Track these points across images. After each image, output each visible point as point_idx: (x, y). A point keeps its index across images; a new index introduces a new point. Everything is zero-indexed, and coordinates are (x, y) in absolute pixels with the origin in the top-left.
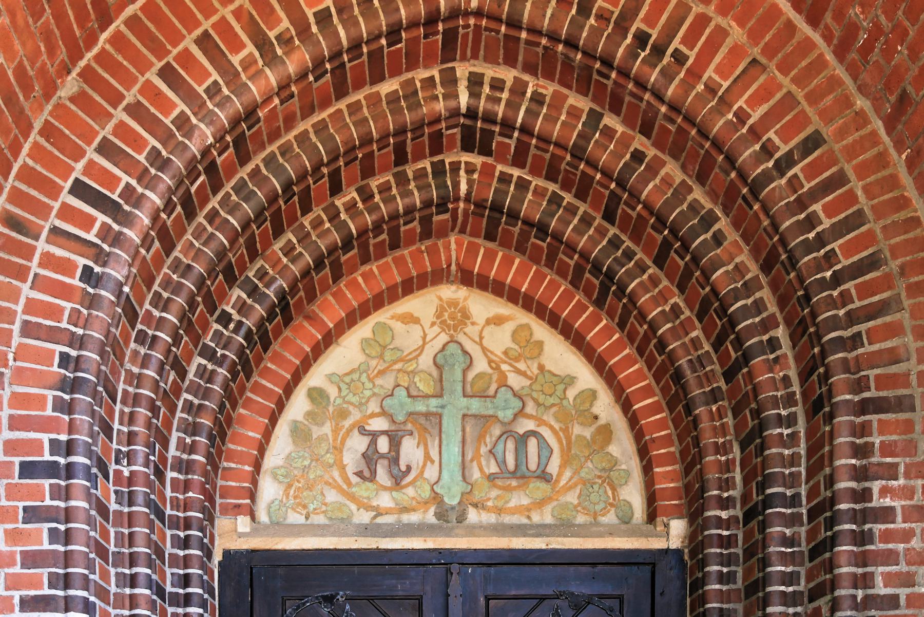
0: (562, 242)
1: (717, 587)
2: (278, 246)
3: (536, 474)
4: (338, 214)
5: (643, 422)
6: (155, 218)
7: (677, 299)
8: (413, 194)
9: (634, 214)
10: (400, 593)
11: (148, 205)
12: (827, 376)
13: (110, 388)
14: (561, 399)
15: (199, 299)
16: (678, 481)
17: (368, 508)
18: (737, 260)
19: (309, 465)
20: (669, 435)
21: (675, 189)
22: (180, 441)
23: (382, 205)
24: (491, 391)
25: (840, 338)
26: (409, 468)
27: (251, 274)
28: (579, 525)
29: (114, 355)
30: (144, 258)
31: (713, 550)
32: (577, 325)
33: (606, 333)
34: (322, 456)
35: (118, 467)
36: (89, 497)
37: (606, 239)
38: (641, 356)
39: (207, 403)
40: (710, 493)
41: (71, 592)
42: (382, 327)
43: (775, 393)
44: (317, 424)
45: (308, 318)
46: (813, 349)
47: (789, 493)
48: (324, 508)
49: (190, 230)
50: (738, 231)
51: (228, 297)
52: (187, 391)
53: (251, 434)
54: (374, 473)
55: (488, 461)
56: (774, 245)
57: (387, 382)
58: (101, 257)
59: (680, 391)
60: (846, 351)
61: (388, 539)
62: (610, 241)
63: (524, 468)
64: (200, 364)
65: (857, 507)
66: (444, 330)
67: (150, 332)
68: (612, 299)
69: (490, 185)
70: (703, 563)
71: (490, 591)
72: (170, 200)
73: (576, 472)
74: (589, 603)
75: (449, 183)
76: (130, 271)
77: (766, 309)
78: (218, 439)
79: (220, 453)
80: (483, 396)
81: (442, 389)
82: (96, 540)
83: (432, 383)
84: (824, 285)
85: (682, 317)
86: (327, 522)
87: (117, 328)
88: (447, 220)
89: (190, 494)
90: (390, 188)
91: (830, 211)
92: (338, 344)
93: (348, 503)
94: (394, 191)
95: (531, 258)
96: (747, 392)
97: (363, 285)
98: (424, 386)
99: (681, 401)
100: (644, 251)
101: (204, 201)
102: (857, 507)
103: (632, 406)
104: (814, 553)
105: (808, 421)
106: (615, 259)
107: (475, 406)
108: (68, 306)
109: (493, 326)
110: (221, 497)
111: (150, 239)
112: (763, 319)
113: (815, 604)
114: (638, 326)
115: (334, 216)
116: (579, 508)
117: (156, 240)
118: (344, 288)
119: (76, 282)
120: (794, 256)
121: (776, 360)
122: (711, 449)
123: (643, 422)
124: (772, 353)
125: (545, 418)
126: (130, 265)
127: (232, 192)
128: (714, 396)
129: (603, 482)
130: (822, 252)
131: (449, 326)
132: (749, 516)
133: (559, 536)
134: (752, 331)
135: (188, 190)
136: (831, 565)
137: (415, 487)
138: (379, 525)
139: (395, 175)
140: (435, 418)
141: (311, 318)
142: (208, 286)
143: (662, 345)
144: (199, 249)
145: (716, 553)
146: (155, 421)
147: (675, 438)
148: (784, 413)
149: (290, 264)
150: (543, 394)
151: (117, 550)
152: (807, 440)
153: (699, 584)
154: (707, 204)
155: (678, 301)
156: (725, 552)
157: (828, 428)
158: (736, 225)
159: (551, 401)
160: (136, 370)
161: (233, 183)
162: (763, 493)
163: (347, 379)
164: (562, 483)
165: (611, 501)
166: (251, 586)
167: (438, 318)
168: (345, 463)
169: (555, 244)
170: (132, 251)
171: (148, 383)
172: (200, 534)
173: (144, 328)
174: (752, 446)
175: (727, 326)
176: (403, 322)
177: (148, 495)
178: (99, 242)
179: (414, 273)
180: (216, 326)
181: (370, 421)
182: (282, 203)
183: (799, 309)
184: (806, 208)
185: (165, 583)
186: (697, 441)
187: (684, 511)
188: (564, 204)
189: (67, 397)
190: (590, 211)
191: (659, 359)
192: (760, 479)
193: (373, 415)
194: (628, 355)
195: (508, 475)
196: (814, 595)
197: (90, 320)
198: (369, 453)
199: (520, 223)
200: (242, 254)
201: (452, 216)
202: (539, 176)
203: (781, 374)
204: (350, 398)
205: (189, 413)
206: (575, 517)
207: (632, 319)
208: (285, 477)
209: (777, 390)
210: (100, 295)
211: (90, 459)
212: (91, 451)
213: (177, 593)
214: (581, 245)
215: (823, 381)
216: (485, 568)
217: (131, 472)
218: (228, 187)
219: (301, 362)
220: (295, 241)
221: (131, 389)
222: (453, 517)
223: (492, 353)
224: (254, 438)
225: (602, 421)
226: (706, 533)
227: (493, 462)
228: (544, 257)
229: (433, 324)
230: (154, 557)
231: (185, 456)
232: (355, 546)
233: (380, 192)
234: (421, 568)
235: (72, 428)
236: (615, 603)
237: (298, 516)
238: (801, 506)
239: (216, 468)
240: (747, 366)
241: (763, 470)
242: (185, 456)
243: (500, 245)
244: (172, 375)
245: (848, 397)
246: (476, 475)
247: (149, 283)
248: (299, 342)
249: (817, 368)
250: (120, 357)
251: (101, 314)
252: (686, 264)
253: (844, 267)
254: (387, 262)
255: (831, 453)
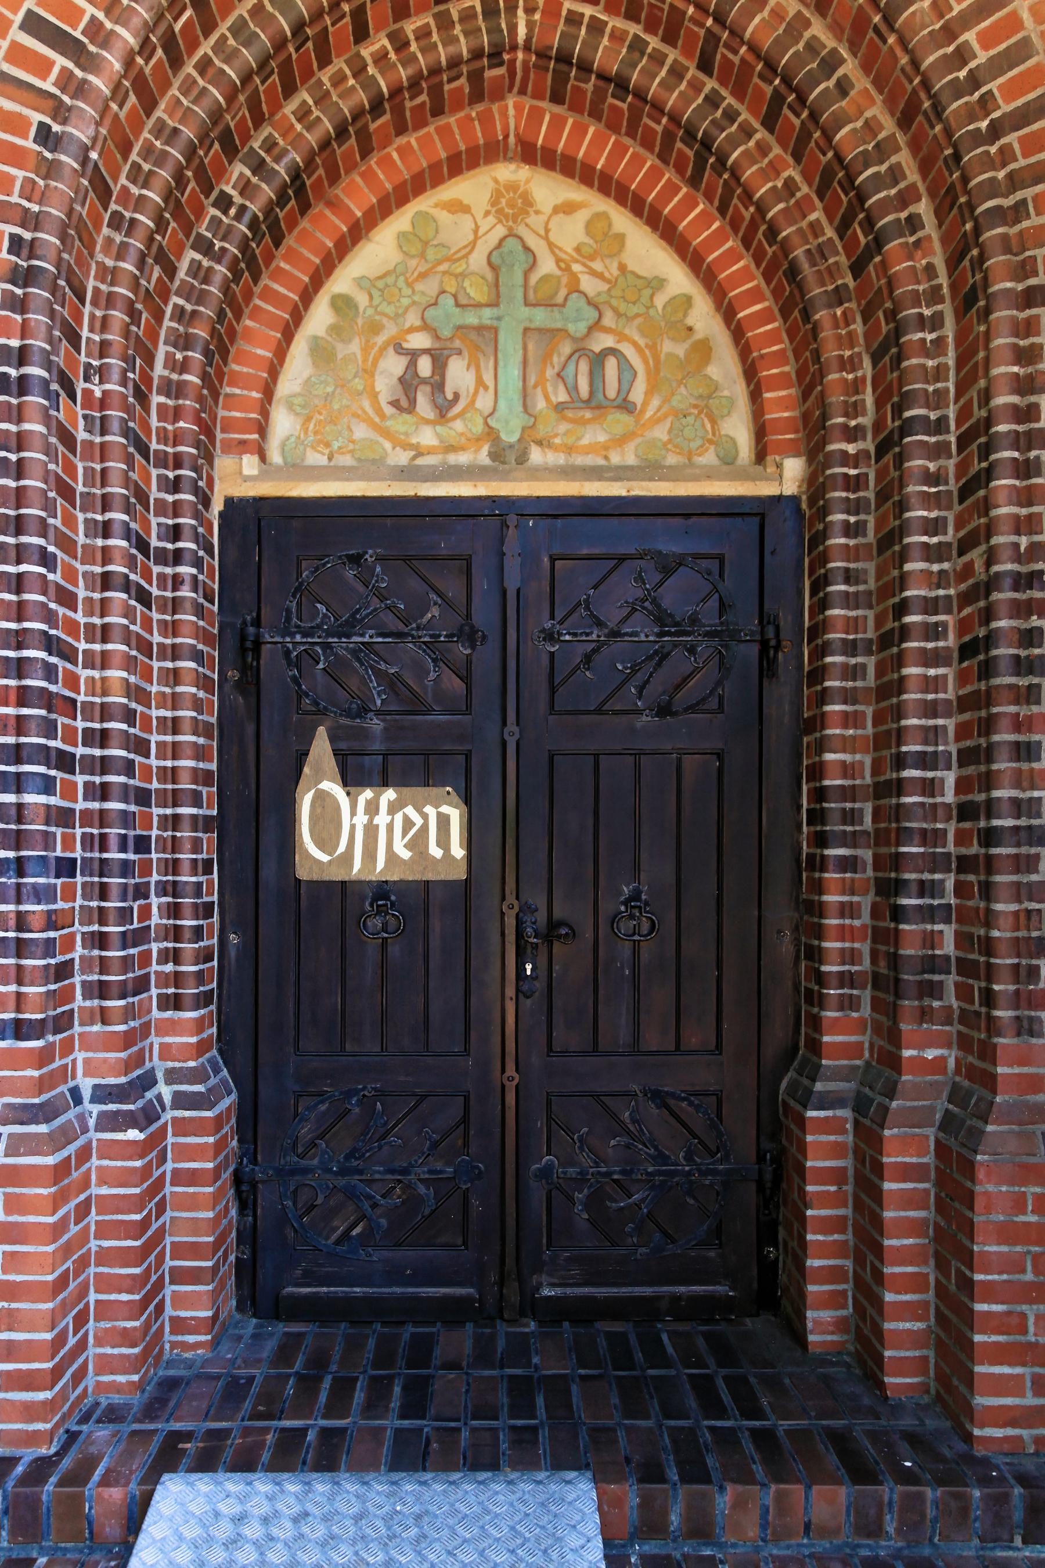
0: (646, 102)
1: (842, 541)
2: (289, 108)
3: (615, 404)
4: (365, 67)
5: (750, 334)
6: (129, 63)
7: (792, 172)
8: (458, 40)
9: (736, 60)
10: (444, 552)
11: (119, 45)
12: (982, 258)
13: (76, 283)
14: (648, 308)
15: (190, 174)
16: (793, 410)
17: (406, 446)
18: (868, 114)
19: (333, 392)
20: (783, 351)
21: (789, 24)
22: (169, 358)
23: (419, 56)
24: (560, 299)
25: (999, 208)
26: (457, 396)
27: (256, 145)
28: (670, 467)
29: (81, 240)
30: (116, 115)
31: (837, 494)
32: (666, 211)
33: (704, 220)
34: (349, 381)
35: (88, 385)
36: (47, 420)
37: (702, 96)
38: (748, 249)
39: (202, 309)
40: (834, 421)
41: (25, 539)
42: (422, 217)
43: (915, 287)
44: (343, 341)
45: (330, 204)
46: (964, 225)
47: (933, 416)
48: (351, 446)
49: (177, 83)
50: (868, 76)
51: (227, 175)
52: (177, 294)
53: (260, 352)
54: (413, 402)
55: (555, 388)
56: (914, 91)
57: (429, 287)
58: (60, 113)
59: (796, 292)
60: (1005, 224)
61: (428, 484)
62: (706, 98)
63: (601, 396)
64: (193, 260)
65: (1020, 428)
66: (500, 221)
67: (127, 215)
68: (710, 175)
69: (556, 28)
70: (824, 512)
71: (557, 550)
72: (146, 40)
73: (666, 400)
74: (680, 564)
75: (504, 26)
76: (97, 132)
77: (905, 177)
78: (217, 356)
79: (220, 375)
80: (550, 305)
81: (498, 296)
82: (56, 474)
83: (486, 289)
84: (979, 140)
85: (799, 195)
86: (353, 463)
87: (83, 205)
88: (503, 76)
89: (182, 424)
90: (429, 34)
91: (987, 40)
92: (369, 240)
93: (381, 440)
94: (435, 37)
95: (609, 126)
96: (880, 288)
97: (399, 162)
98: (476, 292)
99: (797, 305)
100: (750, 109)
101: (193, 45)
102: (1020, 428)
103: (736, 314)
104: (965, 493)
105: (958, 321)
106: (713, 122)
107: (540, 317)
108: (19, 174)
109: (561, 215)
110: (223, 431)
111: (123, 91)
112: (900, 191)
113: (966, 558)
114: (742, 209)
115: (359, 71)
116: (669, 446)
117: (131, 93)
118: (375, 167)
119: (30, 144)
120: (940, 102)
121: (917, 243)
122: (835, 364)
123: (750, 334)
124: (911, 235)
125: (627, 331)
126: (98, 124)
127: (228, 34)
128: (839, 296)
129: (700, 412)
130: (977, 95)
131: (506, 216)
132: (882, 450)
133: (643, 480)
134: (885, 206)
135: (170, 28)
136: (986, 506)
137: (464, 420)
138: (419, 467)
139: (436, 16)
140: (489, 333)
141: (333, 205)
142: (200, 157)
143: (772, 233)
144: (188, 108)
145: (841, 498)
146: (134, 328)
147: (790, 354)
148: (927, 312)
149: (305, 132)
150: (625, 300)
151: (86, 490)
152: (958, 345)
153: (820, 537)
154: (829, 42)
155: (793, 174)
156: (852, 496)
157: (982, 328)
158: (866, 67)
159: (635, 310)
160: (110, 263)
161: (229, 21)
162: (900, 417)
163: (380, 284)
164: (649, 414)
165: (710, 436)
166: (259, 543)
167: (493, 205)
168: (377, 389)
169: (639, 104)
170: (100, 105)
171: (125, 279)
172: (194, 475)
173: (120, 209)
174: (887, 358)
175: (855, 202)
176: (449, 211)
177: (126, 421)
178: (58, 93)
179: (463, 147)
180: (213, 212)
181: (409, 337)
182: (292, 49)
183: (947, 174)
184: (955, 38)
185: (149, 535)
186: (817, 355)
187: (802, 448)
188: (649, 50)
189: (19, 291)
190: (681, 59)
191: (770, 251)
192: (896, 399)
193: (412, 330)
194: (731, 249)
195: (582, 405)
196: (964, 546)
197: (48, 194)
198: (407, 377)
199: (593, 77)
200: (244, 116)
201: (508, 70)
202: (618, 14)
203: (924, 262)
204: (385, 308)
205: (179, 322)
206: (664, 458)
207: (735, 201)
208: (303, 407)
209: (918, 283)
210: (59, 162)
211: (49, 371)
212: (50, 362)
213: (165, 549)
214: (670, 103)
215: (976, 266)
216: (549, 521)
217: (104, 392)
218: (223, 28)
219: (322, 261)
220: (310, 102)
221: (103, 287)
222: (511, 457)
223: (560, 249)
224: (264, 357)
225: (699, 335)
226: (829, 472)
227: (561, 387)
228: (625, 124)
229: (487, 213)
230: (133, 500)
231: (175, 377)
232: (388, 493)
233: (417, 39)
234: (471, 521)
235: (25, 331)
236: (714, 566)
237: (318, 456)
238: (948, 432)
239: (215, 394)
240: (880, 253)
241: (901, 388)
242: (175, 377)
243: (570, 109)
244: (157, 272)
245: (1009, 285)
246: (541, 404)
247: (126, 149)
248: (319, 235)
249: (970, 250)
250: (90, 246)
251: (60, 186)
252: (803, 122)
253: (1004, 115)
254: (429, 133)
255: (987, 360)
